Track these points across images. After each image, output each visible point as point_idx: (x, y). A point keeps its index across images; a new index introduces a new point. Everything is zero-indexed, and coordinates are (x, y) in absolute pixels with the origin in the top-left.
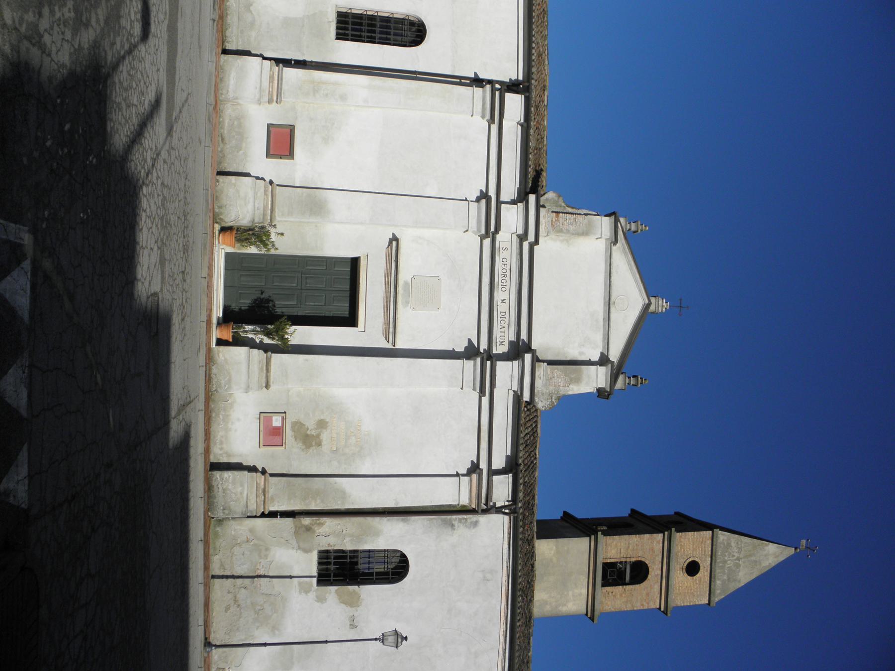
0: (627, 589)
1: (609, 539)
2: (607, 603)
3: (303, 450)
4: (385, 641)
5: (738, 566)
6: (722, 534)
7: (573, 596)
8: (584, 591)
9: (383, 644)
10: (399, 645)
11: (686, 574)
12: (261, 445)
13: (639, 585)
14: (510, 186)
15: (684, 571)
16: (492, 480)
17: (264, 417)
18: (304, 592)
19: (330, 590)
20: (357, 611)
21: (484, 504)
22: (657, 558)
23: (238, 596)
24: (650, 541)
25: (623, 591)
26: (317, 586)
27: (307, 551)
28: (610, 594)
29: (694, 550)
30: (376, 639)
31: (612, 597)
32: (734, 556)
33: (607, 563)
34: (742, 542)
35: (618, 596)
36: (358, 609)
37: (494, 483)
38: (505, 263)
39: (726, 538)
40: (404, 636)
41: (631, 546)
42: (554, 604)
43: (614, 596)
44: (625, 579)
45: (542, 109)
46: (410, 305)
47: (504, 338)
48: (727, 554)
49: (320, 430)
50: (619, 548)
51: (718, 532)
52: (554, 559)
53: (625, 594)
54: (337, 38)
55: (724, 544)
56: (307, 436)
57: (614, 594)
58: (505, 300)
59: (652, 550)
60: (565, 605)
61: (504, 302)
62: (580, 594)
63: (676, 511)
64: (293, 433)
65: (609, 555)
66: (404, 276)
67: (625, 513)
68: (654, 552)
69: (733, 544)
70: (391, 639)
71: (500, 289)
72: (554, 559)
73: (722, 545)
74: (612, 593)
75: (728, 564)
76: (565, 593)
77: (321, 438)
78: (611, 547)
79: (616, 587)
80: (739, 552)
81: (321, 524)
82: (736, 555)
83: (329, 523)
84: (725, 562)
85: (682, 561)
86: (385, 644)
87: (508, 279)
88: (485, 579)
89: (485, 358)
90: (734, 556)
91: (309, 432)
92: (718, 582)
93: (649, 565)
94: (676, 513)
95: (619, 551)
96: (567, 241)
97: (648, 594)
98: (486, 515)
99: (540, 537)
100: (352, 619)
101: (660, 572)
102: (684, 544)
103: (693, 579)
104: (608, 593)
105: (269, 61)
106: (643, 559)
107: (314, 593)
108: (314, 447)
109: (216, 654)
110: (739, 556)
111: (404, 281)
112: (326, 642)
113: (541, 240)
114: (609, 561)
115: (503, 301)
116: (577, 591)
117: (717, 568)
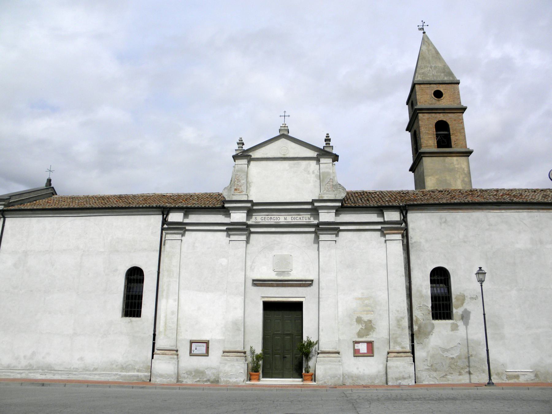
0: (453, 133)
1: (424, 145)
2: (462, 144)
3: (374, 331)
4: (482, 280)
5: (435, 67)
6: (417, 78)
7: (458, 164)
8: (455, 158)
9: (484, 281)
10: (484, 272)
11: (442, 98)
12: (372, 355)
13: (450, 126)
14: (219, 218)
15: (440, 99)
16: (387, 221)
17: (357, 353)
18: (458, 328)
19: (456, 312)
20: (467, 296)
21: (401, 225)
22: (433, 116)
23: (461, 367)
24: (423, 121)
25: (453, 135)
26: (453, 320)
27: (433, 326)
28: (455, 142)
29: (427, 94)
30: (482, 286)
31: (458, 141)
32: (430, 70)
33: (437, 145)
34: (421, 66)
35: (457, 138)
36: (466, 295)
37: (389, 220)
38: (264, 218)
39: (419, 76)
40: (479, 269)
41: (427, 132)
42: (463, 176)
43: (457, 140)
44: (446, 134)
45: (175, 197)
46: (289, 272)
47: (306, 218)
48: (429, 75)
49: (362, 321)
50: (428, 139)
51: (416, 81)
52: (437, 177)
53: (455, 133)
54: (140, 316)
55: (423, 76)
56: (366, 328)
57: (456, 140)
58: (285, 218)
59: (428, 119)
60: (464, 169)
61: (286, 218)
62: (457, 160)
63: (406, 104)
64: (364, 337)
65: (433, 144)
66: (273, 276)
67: (408, 134)
68: (430, 118)
69: (423, 71)
70: (481, 276)
71: (279, 221)
72: (437, 177)
73: (424, 78)
74: (455, 141)
75: (435, 73)
76: (457, 169)
77: (367, 320)
78: (428, 144)
79: (452, 139)
80: (427, 67)
81: (417, 319)
82: (429, 69)
83: (416, 313)
84: (433, 75)
85: (434, 101)
86: (484, 280)
87: (273, 217)
88: (445, 222)
89: (318, 228)
90: (430, 70)
91: (363, 328)
92: (446, 79)
93: (438, 120)
94: (407, 104)
95: (430, 139)
96: (250, 183)
97: (455, 120)
98: (408, 224)
99: (424, 187)
100: (472, 298)
101: (441, 114)
102: (424, 100)
103: (444, 94)
104: (456, 144)
105: (154, 355)
106: (434, 124)
107: (458, 321)
108: (372, 324)
109: (495, 380)
110: (429, 67)
111: (276, 275)
112: (484, 314)
113: (250, 199)
114: (436, 144)
115: (285, 219)
116: (455, 163)
117: (437, 80)
